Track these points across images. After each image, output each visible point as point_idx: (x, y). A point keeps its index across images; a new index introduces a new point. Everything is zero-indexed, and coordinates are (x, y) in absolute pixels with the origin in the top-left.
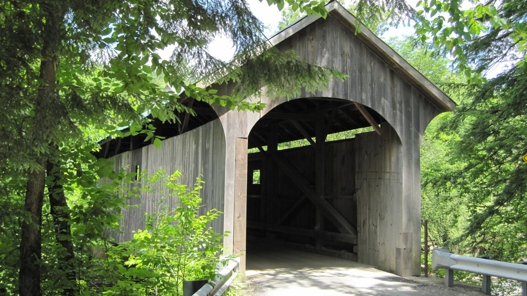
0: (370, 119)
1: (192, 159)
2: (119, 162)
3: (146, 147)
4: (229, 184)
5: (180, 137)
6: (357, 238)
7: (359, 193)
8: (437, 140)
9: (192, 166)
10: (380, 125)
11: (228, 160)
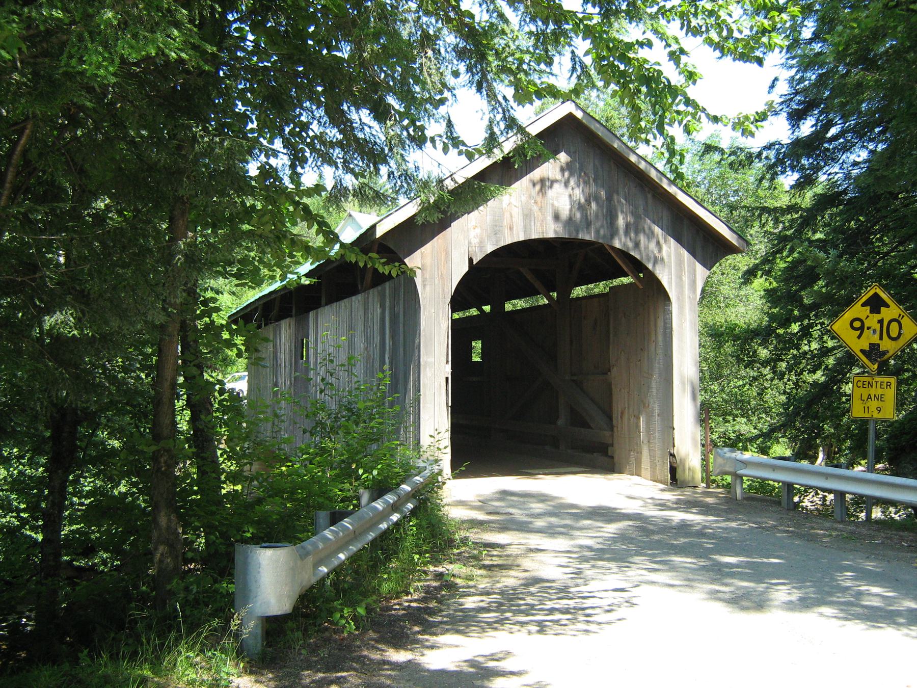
0: (628, 266)
1: (377, 328)
2: (278, 331)
3: (315, 311)
4: (426, 362)
5: (360, 297)
6: (612, 436)
7: (614, 371)
8: (748, 288)
9: (377, 339)
10: (641, 275)
11: (424, 330)
